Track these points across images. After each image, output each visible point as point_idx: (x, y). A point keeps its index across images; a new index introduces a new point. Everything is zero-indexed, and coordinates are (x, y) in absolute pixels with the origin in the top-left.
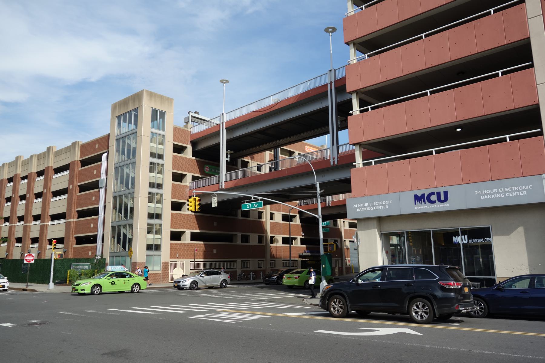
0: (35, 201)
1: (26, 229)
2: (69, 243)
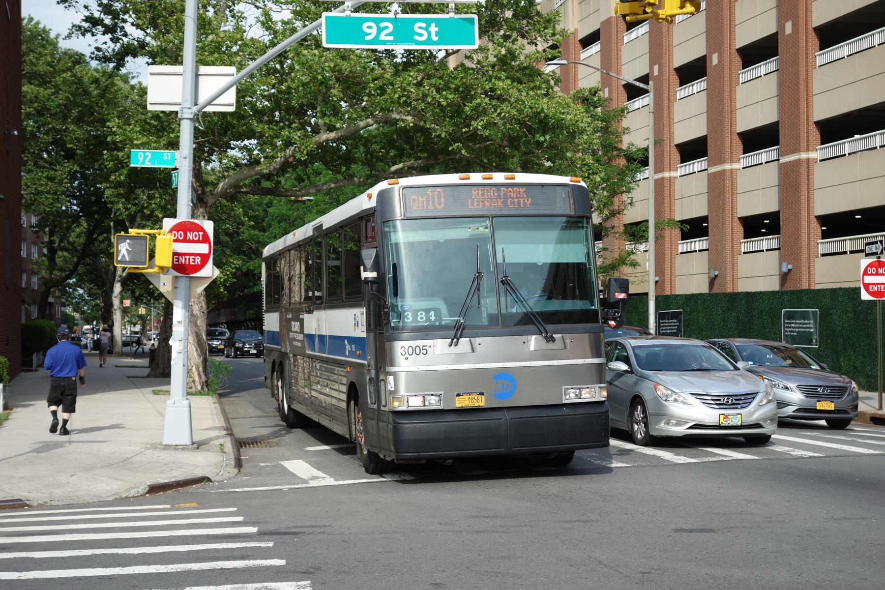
0: (679, 95)
1: (719, 188)
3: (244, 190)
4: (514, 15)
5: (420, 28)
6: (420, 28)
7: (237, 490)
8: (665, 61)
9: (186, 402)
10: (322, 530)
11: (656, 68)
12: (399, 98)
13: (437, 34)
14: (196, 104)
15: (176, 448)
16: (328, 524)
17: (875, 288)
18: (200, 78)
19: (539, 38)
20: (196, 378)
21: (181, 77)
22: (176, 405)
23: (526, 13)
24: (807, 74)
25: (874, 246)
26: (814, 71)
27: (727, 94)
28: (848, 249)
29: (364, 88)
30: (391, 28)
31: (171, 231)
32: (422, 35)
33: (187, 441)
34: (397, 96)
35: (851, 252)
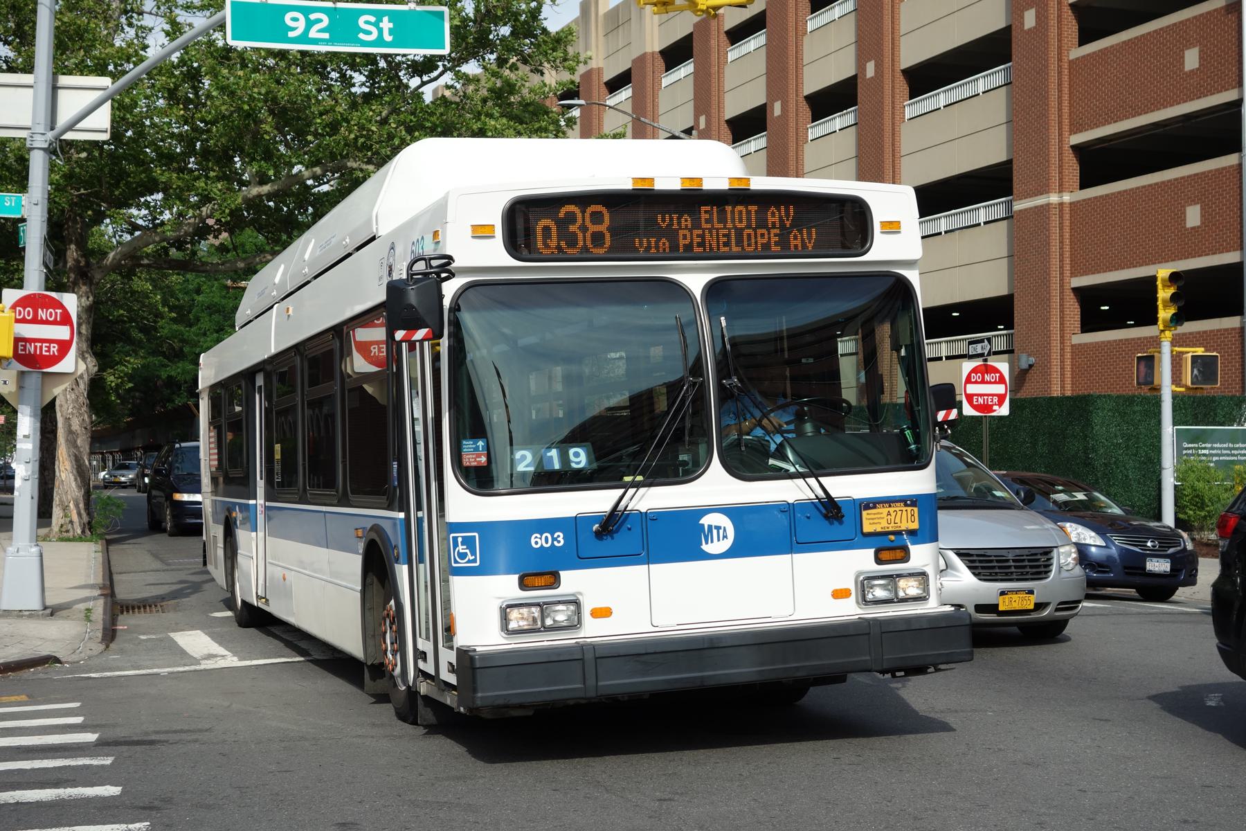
2: (1047, 321)
3: (146, 261)
4: (512, 33)
5: (367, 22)
6: (367, 22)
7: (93, 675)
8: (714, 111)
9: (35, 550)
10: (194, 737)
11: (702, 120)
12: (356, 138)
13: (391, 32)
14: (52, 129)
15: (20, 614)
16: (207, 727)
17: (981, 400)
18: (60, 91)
19: (546, 64)
20: (75, 518)
21: (31, 90)
22: (21, 553)
23: (528, 27)
24: (893, 129)
25: (979, 345)
26: (903, 126)
27: (792, 154)
28: (944, 354)
29: (309, 125)
30: (326, 21)
31: (14, 307)
32: (369, 33)
33: (35, 604)
34: (352, 136)
35: (948, 358)
